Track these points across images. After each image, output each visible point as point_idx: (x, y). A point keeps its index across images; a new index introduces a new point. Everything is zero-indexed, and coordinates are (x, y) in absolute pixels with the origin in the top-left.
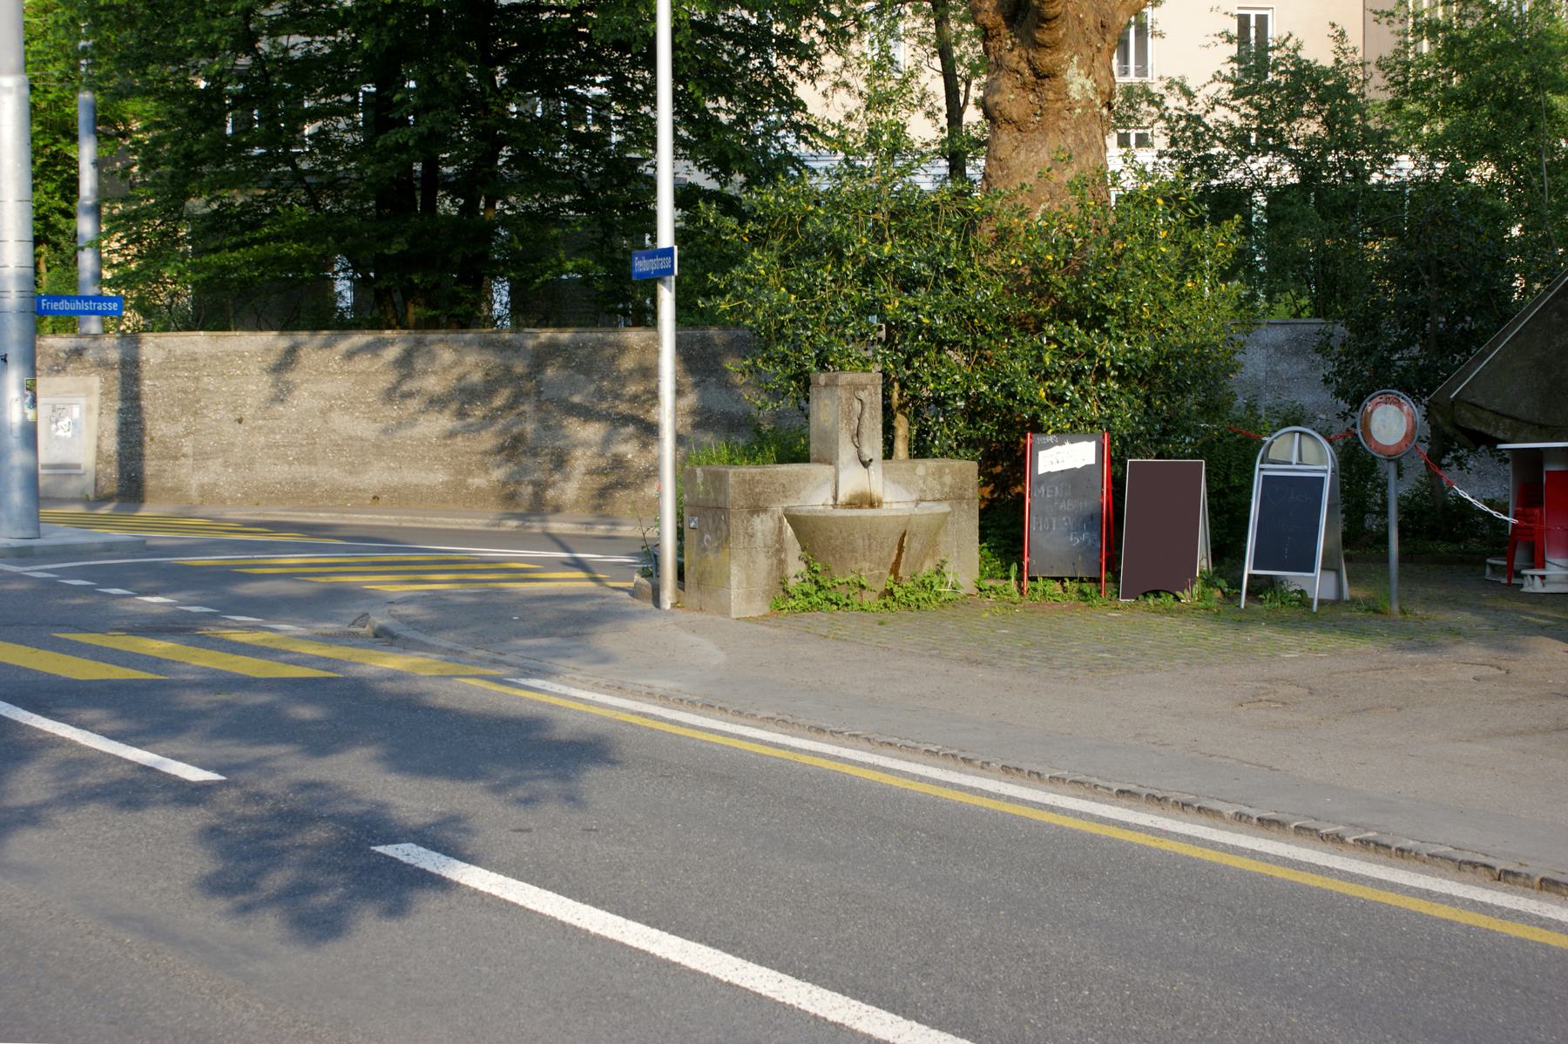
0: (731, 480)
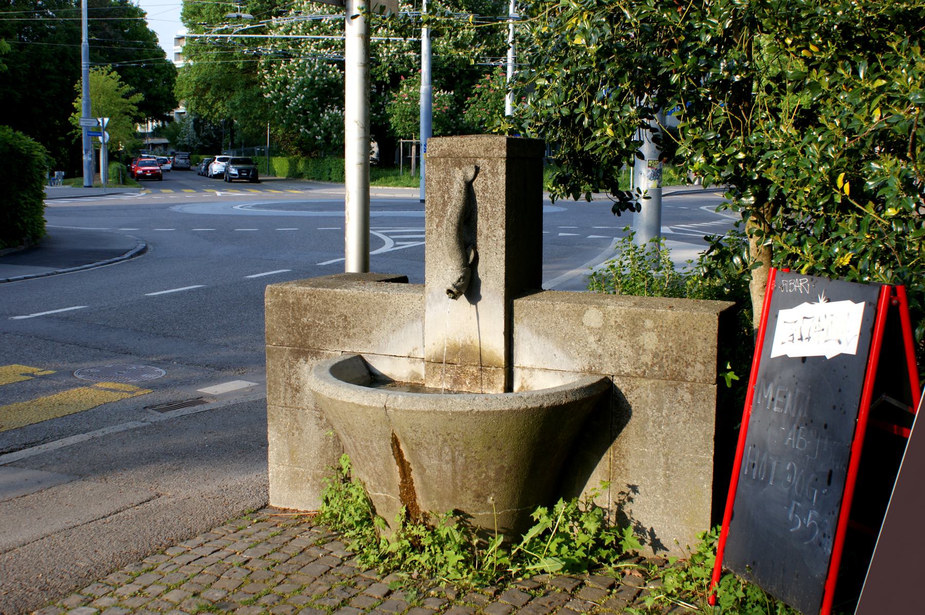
0: (268, 301)
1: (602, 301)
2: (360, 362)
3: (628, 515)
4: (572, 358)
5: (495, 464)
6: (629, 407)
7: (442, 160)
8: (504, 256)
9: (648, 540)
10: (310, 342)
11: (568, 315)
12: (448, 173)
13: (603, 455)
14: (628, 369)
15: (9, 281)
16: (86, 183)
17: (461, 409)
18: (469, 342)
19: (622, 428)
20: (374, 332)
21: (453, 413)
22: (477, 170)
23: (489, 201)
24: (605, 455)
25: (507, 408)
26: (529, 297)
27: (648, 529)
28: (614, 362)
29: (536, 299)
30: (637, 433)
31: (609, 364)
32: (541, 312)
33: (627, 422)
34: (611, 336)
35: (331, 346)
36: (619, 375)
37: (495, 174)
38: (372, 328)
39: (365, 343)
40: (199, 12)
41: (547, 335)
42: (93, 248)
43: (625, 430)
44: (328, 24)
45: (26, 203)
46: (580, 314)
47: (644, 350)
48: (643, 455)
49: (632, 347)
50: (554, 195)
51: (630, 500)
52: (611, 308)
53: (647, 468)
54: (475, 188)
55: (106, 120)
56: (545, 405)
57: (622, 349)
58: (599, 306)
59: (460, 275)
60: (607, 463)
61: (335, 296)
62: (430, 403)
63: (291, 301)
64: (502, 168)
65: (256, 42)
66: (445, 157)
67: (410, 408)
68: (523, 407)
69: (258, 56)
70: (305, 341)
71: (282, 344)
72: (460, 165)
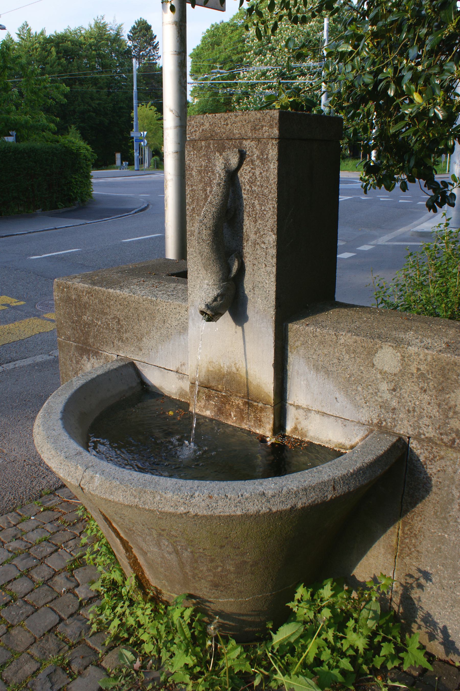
1: (402, 335)
2: (131, 370)
3: (416, 602)
4: (358, 407)
5: (232, 560)
6: (429, 479)
7: (203, 143)
8: (274, 270)
9: (440, 635)
10: (91, 340)
11: (354, 352)
12: (209, 159)
13: (389, 527)
14: (430, 433)
15: (56, 229)
16: (136, 168)
17: (171, 510)
18: (234, 369)
19: (416, 503)
20: (144, 339)
21: (161, 513)
22: (242, 156)
23: (257, 197)
24: (392, 529)
25: (239, 513)
26: (311, 319)
27: (441, 626)
28: (413, 420)
29: (316, 324)
30: (435, 513)
31: (406, 422)
32: (321, 343)
33: (423, 498)
34: (409, 387)
35: (108, 348)
36: (418, 438)
37: (264, 161)
38: (143, 335)
39: (137, 349)
40: (200, 71)
41: (327, 373)
42: (115, 207)
43: (420, 505)
44: (270, 75)
45: (76, 181)
46: (371, 353)
47: (455, 413)
48: (442, 540)
49: (439, 405)
50: (367, 185)
51: (420, 586)
52: (412, 350)
53: (446, 558)
54: (241, 179)
55: (145, 133)
56: (299, 505)
57: (425, 405)
58: (398, 343)
59: (215, 293)
60: (394, 538)
61: (109, 297)
62: (132, 495)
63: (73, 297)
64: (273, 152)
65: (230, 86)
66: (206, 139)
67: (107, 496)
68: (264, 510)
69: (232, 95)
70: (86, 339)
71: (69, 339)
72: (221, 149)
